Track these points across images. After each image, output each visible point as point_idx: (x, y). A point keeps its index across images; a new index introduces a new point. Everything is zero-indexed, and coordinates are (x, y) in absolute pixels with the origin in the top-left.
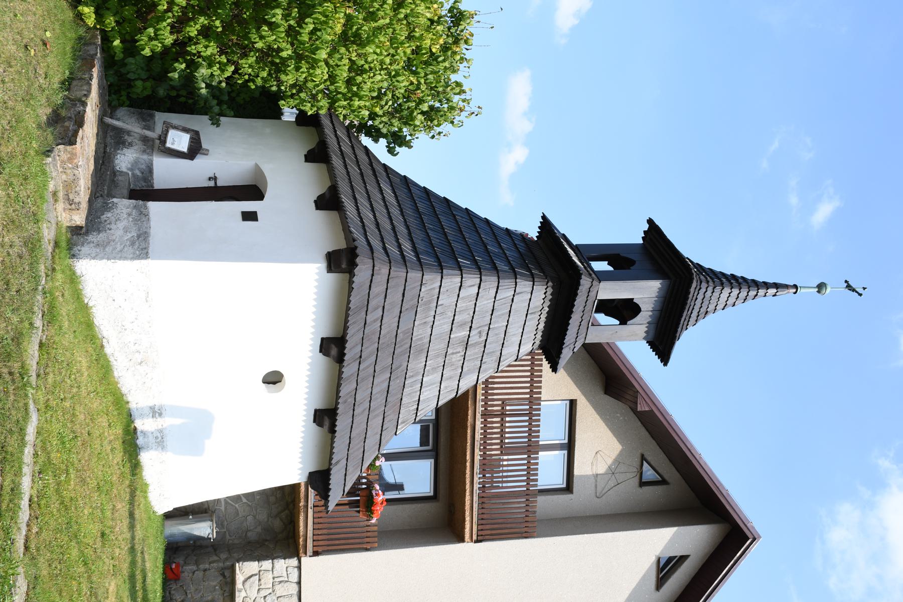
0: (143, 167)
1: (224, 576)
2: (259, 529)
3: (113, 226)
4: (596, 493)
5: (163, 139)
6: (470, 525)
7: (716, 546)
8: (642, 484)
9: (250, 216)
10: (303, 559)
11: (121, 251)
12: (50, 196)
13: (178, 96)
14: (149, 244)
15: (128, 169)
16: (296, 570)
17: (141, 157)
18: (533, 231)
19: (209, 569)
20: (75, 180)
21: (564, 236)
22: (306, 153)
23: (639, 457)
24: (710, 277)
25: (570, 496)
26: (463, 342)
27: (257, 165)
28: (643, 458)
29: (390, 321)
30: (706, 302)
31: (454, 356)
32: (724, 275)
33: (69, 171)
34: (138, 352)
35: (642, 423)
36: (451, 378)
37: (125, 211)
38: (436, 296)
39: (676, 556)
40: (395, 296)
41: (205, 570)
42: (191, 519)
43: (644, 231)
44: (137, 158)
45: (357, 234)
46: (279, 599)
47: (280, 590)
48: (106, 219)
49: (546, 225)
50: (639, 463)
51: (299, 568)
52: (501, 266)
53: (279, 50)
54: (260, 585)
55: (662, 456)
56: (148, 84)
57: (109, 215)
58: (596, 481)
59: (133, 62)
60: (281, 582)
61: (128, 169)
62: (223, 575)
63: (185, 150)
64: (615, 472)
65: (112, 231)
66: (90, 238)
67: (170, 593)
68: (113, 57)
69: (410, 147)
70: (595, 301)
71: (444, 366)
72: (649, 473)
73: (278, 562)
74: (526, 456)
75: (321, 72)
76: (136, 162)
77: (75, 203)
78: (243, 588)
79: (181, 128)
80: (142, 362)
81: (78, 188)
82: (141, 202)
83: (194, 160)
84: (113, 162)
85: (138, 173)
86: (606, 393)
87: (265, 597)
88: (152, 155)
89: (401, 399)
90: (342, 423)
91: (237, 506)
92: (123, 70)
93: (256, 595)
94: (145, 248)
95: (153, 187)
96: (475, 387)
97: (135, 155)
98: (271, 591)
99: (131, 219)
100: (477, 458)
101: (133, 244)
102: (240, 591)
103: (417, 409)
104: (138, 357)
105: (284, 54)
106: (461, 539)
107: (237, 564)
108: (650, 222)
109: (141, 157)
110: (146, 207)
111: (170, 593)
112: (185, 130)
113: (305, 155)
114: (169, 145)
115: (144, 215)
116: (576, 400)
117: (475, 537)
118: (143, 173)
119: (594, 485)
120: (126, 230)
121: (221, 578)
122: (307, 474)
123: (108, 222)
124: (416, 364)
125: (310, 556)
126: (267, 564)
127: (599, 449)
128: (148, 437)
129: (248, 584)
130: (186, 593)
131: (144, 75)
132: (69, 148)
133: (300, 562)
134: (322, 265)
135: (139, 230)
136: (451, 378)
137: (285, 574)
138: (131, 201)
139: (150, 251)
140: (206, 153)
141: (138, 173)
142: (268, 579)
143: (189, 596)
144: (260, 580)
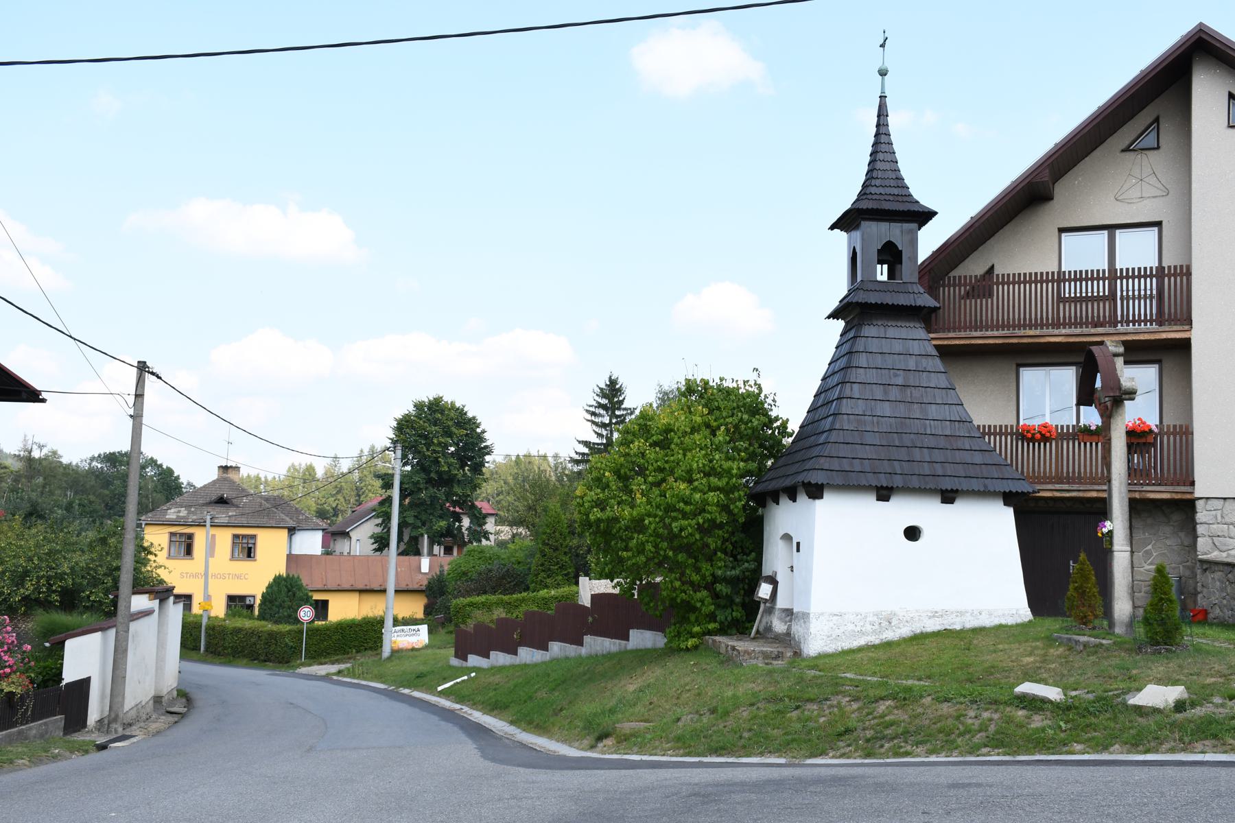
0: (784, 614)
2: (1182, 535)
7: (1221, 63)
12: (767, 666)
13: (744, 589)
15: (785, 624)
16: (1210, 502)
18: (840, 324)
20: (763, 652)
21: (840, 302)
23: (1124, 154)
27: (781, 538)
28: (1127, 150)
30: (887, 183)
33: (757, 656)
34: (880, 624)
35: (1086, 156)
38: (856, 416)
40: (844, 451)
44: (778, 618)
49: (834, 315)
50: (1132, 153)
53: (698, 524)
55: (1125, 128)
56: (735, 608)
58: (1149, 197)
59: (719, 617)
60: (1222, 517)
61: (785, 624)
63: (771, 586)
67: (1214, 619)
68: (718, 629)
69: (788, 420)
75: (712, 497)
76: (781, 619)
78: (1226, 553)
84: (780, 634)
86: (1052, 199)
89: (946, 435)
91: (1155, 554)
92: (726, 623)
104: (885, 624)
105: (701, 521)
107: (1200, 557)
108: (832, 228)
111: (1214, 619)
114: (768, 597)
116: (1058, 228)
117: (1186, 327)
119: (1153, 200)
122: (1005, 507)
124: (916, 426)
127: (1112, 198)
131: (729, 611)
134: (818, 502)
137: (1214, 513)
143: (1217, 601)
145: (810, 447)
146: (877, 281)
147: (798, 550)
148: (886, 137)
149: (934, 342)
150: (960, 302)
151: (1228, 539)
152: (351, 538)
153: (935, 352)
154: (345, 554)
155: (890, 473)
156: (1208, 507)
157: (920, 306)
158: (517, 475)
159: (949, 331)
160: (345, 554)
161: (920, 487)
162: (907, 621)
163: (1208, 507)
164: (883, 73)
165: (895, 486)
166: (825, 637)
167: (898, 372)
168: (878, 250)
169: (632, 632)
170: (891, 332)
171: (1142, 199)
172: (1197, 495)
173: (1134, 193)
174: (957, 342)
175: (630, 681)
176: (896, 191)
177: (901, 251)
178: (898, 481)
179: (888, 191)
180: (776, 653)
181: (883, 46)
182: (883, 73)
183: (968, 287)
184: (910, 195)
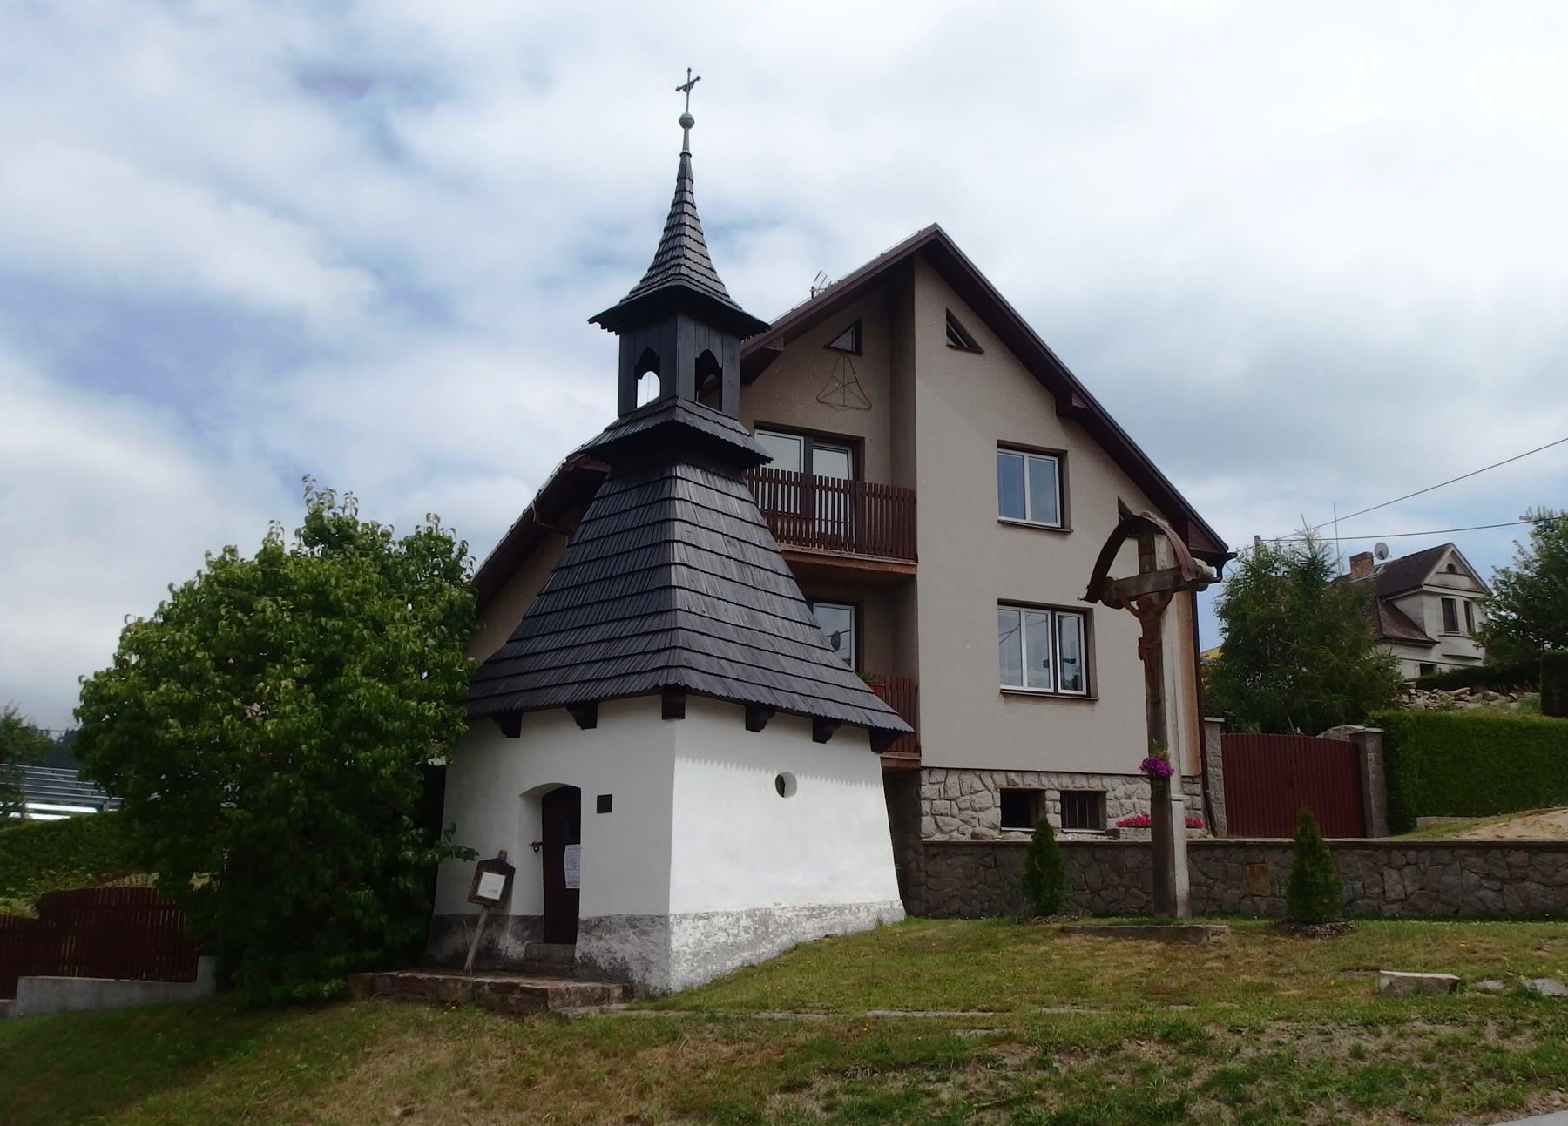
1: (937, 854)
3: (619, 956)
4: (865, 410)
5: (488, 903)
6: (895, 565)
8: (857, 351)
9: (605, 804)
10: (923, 764)
11: (656, 944)
14: (645, 915)
15: (523, 943)
17: (510, 928)
19: (927, 872)
22: (505, 736)
24: (671, 259)
25: (867, 441)
26: (741, 567)
28: (828, 347)
29: (733, 651)
31: (755, 578)
32: (664, 242)
33: (573, 998)
36: (776, 583)
37: (594, 942)
39: (947, 326)
41: (928, 876)
42: (454, 1010)
43: (602, 328)
44: (512, 933)
45: (645, 682)
46: (963, 793)
47: (953, 793)
48: (607, 963)
51: (931, 769)
52: (653, 515)
54: (947, 815)
57: (601, 960)
58: (852, 408)
60: (945, 791)
62: (934, 856)
63: (503, 878)
64: (846, 390)
65: (627, 955)
66: (637, 978)
70: (698, 406)
71: (766, 591)
72: (846, 342)
73: (923, 793)
74: (780, 486)
76: (517, 936)
77: (603, 993)
79: (476, 882)
80: (765, 927)
81: (589, 989)
82: (581, 927)
83: (515, 866)
85: (526, 933)
87: (960, 809)
88: (507, 916)
90: (834, 712)
93: (957, 820)
94: (652, 919)
95: (541, 917)
96: (784, 553)
97: (508, 937)
98: (953, 803)
99: (608, 936)
100: (854, 555)
101: (645, 933)
102: (951, 837)
103: (808, 625)
106: (913, 578)
109: (510, 928)
110: (588, 921)
112: (478, 877)
113: (508, 737)
114: (497, 897)
115: (599, 924)
117: (911, 562)
118: (527, 928)
120: (624, 940)
121: (938, 857)
123: (612, 961)
125: (921, 756)
126: (925, 806)
128: (836, 923)
129: (947, 829)
130: (953, 896)
132: (550, 996)
133: (925, 768)
134: (677, 723)
135: (624, 926)
136: (776, 583)
137: (937, 786)
138: (578, 938)
139: (657, 914)
140: (503, 854)
141: (526, 933)
142: (941, 805)
143: (956, 893)
144: (942, 815)
145: (498, 678)
151: (950, 818)
156: (933, 780)
158: (429, 530)
162: (785, 925)
163: (933, 780)
166: (690, 957)
168: (696, 359)
169: (23, 982)
171: (844, 408)
172: (923, 764)
173: (837, 399)
177: (721, 369)
180: (600, 991)
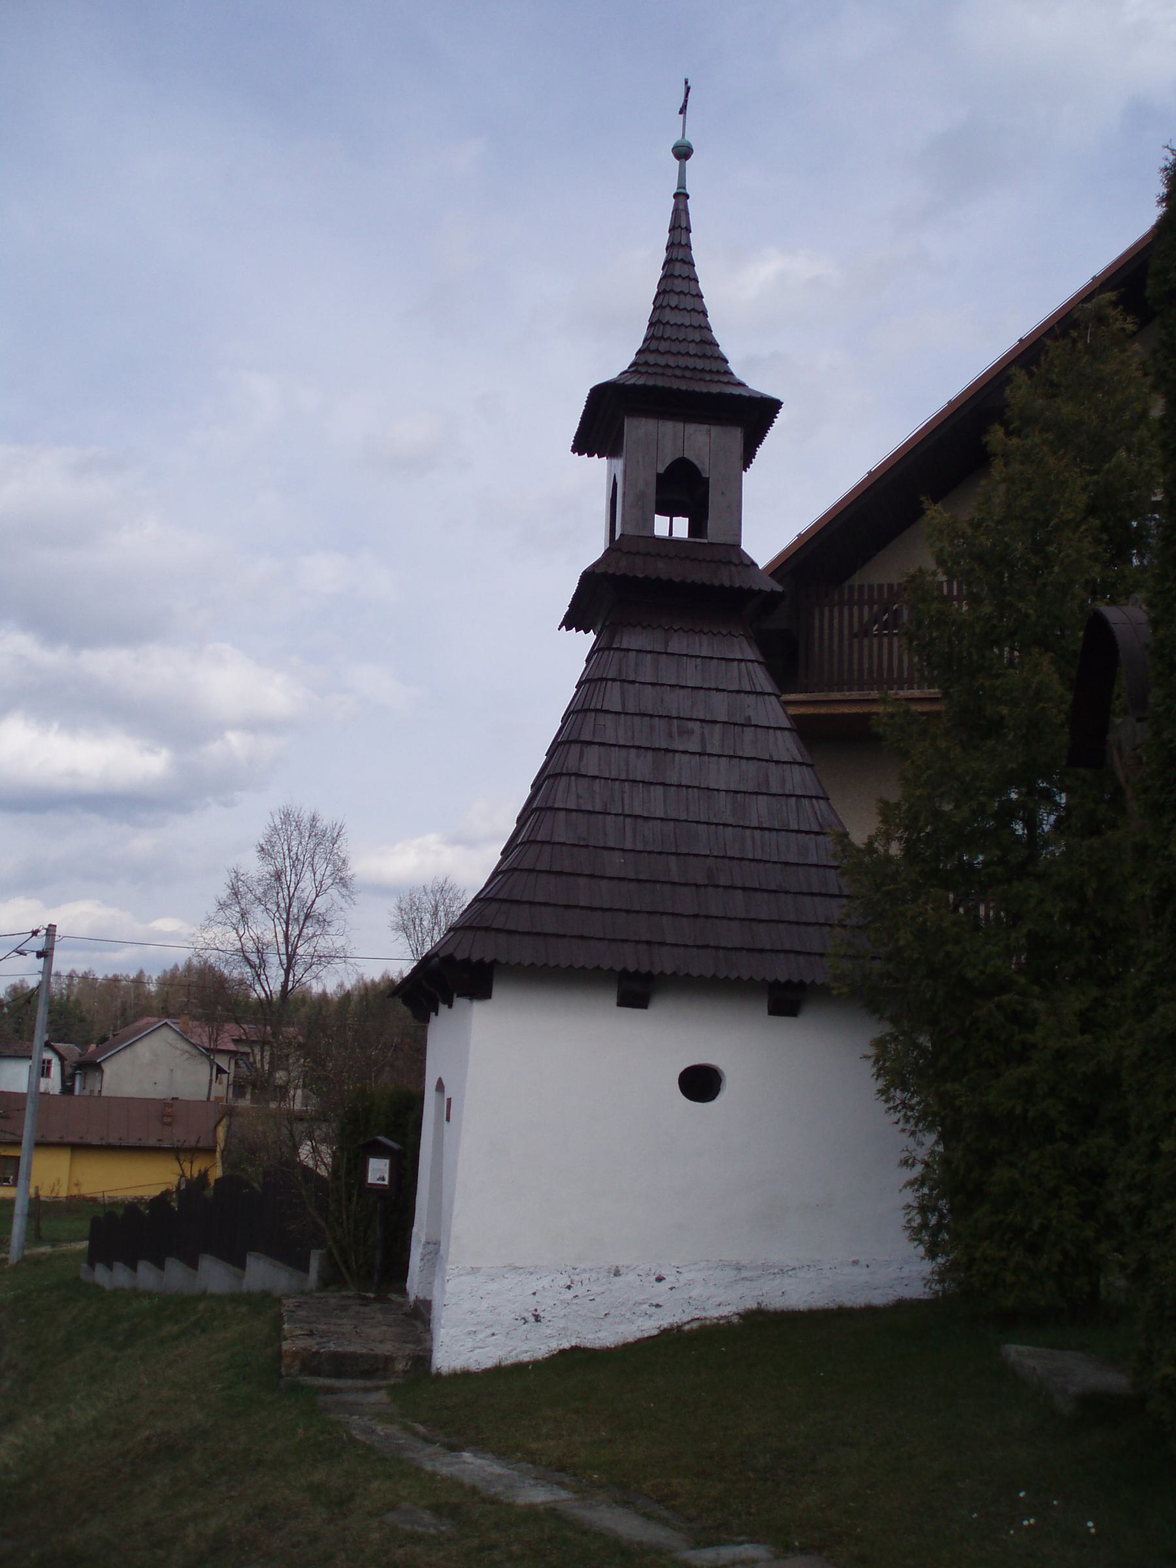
18: (586, 640)
146: (654, 537)
147: (448, 1119)
148: (686, 267)
149: (792, 710)
150: (851, 645)
152: (103, 1071)
153: (787, 724)
154: (96, 1093)
155: (648, 943)
157: (740, 588)
159: (831, 690)
160: (96, 1093)
161: (714, 976)
164: (683, 153)
165: (656, 972)
167: (690, 724)
168: (659, 476)
170: (678, 644)
174: (846, 710)
175: (762, 1298)
176: (700, 364)
178: (665, 962)
179: (682, 361)
181: (683, 111)
182: (683, 153)
183: (876, 607)
184: (729, 373)
